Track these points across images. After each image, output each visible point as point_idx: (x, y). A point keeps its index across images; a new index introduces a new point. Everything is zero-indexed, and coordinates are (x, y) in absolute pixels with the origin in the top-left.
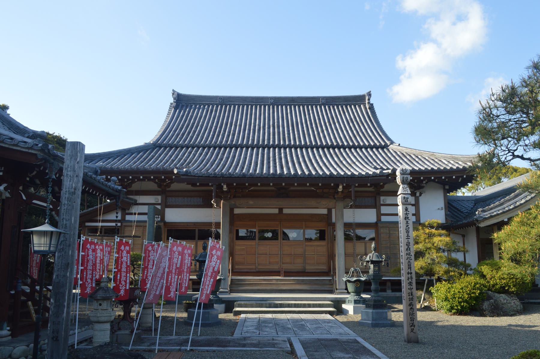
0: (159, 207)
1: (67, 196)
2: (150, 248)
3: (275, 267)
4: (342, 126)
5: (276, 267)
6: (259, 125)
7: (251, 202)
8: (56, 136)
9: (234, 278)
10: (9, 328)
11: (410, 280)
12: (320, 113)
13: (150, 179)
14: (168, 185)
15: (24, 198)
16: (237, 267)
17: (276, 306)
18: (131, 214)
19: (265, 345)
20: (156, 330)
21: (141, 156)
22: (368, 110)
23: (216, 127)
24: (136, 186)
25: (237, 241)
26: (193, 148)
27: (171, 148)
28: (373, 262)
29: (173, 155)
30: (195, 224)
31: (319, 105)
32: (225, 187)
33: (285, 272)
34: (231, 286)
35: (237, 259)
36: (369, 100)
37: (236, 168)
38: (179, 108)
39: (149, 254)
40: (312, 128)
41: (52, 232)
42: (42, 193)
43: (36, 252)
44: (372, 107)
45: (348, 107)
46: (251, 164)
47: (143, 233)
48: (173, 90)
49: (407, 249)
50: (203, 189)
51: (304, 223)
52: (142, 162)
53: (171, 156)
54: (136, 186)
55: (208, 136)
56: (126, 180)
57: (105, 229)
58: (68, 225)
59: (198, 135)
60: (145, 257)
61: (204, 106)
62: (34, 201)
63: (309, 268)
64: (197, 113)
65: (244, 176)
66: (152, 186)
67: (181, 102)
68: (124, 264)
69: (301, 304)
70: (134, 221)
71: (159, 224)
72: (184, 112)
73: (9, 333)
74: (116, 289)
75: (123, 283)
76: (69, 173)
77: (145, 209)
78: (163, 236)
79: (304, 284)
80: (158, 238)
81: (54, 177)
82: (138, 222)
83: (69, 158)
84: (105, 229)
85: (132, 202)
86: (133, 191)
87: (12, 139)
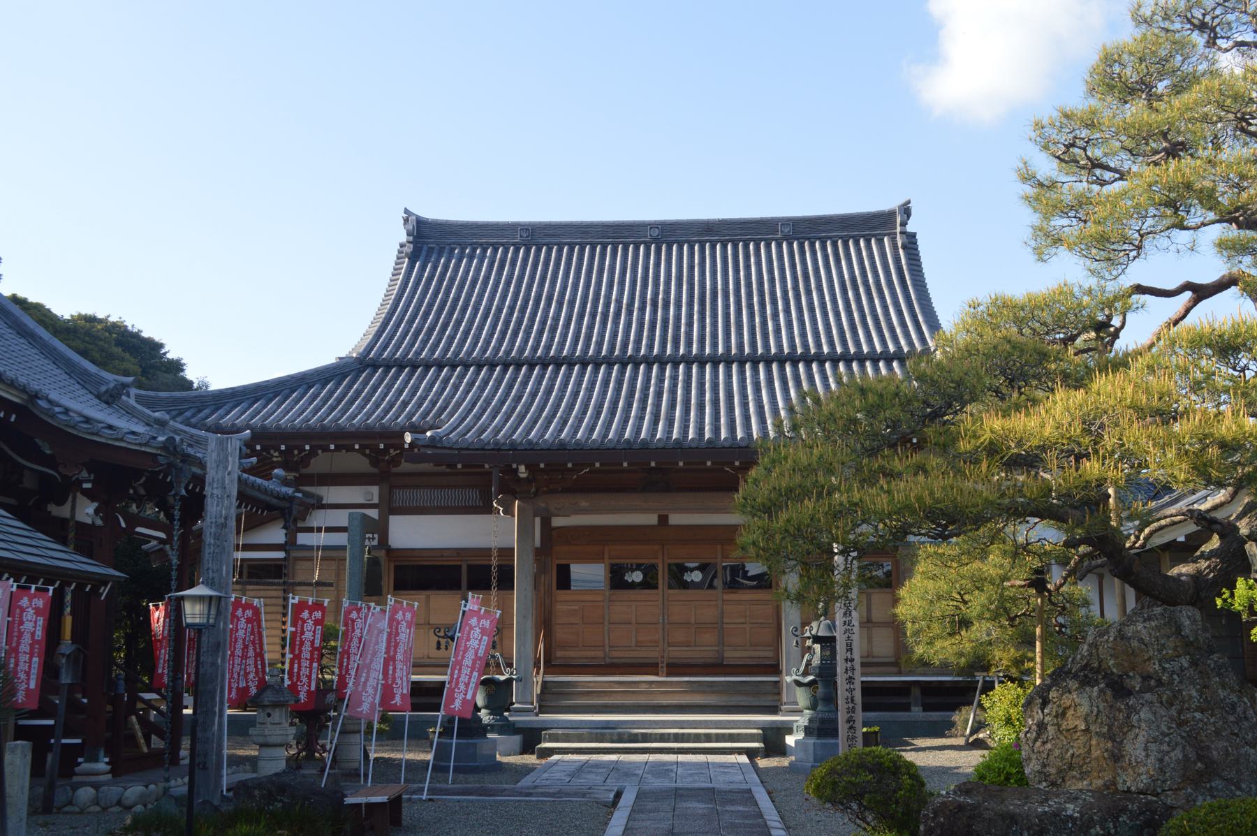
0: (374, 513)
1: (213, 530)
2: (354, 615)
3: (651, 654)
4: (827, 298)
5: (652, 654)
6: (619, 301)
7: (584, 504)
8: (114, 325)
9: (550, 678)
10: (107, 760)
11: (850, 673)
12: (775, 264)
13: (350, 449)
14: (395, 461)
15: (123, 525)
16: (559, 654)
17: (634, 738)
18: (310, 530)
19: (568, 795)
20: (366, 775)
21: (331, 393)
22: (901, 251)
23: (512, 308)
24: (319, 464)
25: (559, 592)
26: (454, 367)
27: (401, 368)
28: (817, 639)
29: (405, 387)
30: (459, 552)
31: (776, 240)
32: (522, 468)
33: (669, 665)
34: (541, 697)
35: (560, 634)
36: (904, 224)
37: (548, 427)
38: (422, 258)
39: (21, 617)
40: (750, 306)
41: (211, 597)
42: (148, 512)
43: (188, 625)
44: (911, 243)
45: (851, 243)
46: (585, 413)
47: (338, 575)
48: (406, 211)
49: (845, 614)
50: (476, 475)
51: (719, 547)
52: (332, 409)
53: (400, 392)
54: (319, 464)
55: (491, 335)
56: (296, 452)
57: (250, 567)
58: (216, 580)
59: (466, 333)
60: (346, 633)
61: (485, 251)
62: (139, 529)
63: (733, 655)
64: (465, 269)
65: (562, 446)
66: (357, 462)
67: (429, 241)
68: (307, 644)
69: (689, 734)
70: (318, 547)
71: (374, 553)
72: (435, 268)
73: (109, 767)
74: (293, 688)
75: (304, 679)
76: (215, 492)
77: (340, 518)
78: (384, 583)
79: (713, 692)
80: (372, 589)
81: (183, 492)
82: (325, 548)
83: (214, 465)
84: (250, 567)
85: (311, 501)
86: (312, 476)
87: (110, 427)
